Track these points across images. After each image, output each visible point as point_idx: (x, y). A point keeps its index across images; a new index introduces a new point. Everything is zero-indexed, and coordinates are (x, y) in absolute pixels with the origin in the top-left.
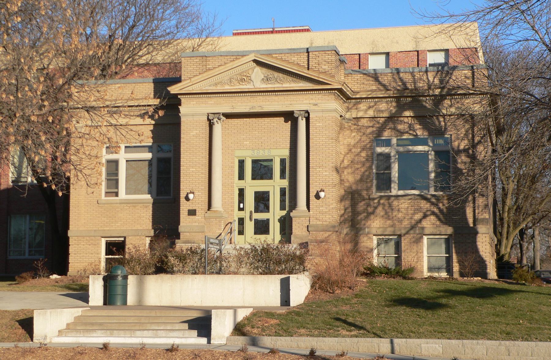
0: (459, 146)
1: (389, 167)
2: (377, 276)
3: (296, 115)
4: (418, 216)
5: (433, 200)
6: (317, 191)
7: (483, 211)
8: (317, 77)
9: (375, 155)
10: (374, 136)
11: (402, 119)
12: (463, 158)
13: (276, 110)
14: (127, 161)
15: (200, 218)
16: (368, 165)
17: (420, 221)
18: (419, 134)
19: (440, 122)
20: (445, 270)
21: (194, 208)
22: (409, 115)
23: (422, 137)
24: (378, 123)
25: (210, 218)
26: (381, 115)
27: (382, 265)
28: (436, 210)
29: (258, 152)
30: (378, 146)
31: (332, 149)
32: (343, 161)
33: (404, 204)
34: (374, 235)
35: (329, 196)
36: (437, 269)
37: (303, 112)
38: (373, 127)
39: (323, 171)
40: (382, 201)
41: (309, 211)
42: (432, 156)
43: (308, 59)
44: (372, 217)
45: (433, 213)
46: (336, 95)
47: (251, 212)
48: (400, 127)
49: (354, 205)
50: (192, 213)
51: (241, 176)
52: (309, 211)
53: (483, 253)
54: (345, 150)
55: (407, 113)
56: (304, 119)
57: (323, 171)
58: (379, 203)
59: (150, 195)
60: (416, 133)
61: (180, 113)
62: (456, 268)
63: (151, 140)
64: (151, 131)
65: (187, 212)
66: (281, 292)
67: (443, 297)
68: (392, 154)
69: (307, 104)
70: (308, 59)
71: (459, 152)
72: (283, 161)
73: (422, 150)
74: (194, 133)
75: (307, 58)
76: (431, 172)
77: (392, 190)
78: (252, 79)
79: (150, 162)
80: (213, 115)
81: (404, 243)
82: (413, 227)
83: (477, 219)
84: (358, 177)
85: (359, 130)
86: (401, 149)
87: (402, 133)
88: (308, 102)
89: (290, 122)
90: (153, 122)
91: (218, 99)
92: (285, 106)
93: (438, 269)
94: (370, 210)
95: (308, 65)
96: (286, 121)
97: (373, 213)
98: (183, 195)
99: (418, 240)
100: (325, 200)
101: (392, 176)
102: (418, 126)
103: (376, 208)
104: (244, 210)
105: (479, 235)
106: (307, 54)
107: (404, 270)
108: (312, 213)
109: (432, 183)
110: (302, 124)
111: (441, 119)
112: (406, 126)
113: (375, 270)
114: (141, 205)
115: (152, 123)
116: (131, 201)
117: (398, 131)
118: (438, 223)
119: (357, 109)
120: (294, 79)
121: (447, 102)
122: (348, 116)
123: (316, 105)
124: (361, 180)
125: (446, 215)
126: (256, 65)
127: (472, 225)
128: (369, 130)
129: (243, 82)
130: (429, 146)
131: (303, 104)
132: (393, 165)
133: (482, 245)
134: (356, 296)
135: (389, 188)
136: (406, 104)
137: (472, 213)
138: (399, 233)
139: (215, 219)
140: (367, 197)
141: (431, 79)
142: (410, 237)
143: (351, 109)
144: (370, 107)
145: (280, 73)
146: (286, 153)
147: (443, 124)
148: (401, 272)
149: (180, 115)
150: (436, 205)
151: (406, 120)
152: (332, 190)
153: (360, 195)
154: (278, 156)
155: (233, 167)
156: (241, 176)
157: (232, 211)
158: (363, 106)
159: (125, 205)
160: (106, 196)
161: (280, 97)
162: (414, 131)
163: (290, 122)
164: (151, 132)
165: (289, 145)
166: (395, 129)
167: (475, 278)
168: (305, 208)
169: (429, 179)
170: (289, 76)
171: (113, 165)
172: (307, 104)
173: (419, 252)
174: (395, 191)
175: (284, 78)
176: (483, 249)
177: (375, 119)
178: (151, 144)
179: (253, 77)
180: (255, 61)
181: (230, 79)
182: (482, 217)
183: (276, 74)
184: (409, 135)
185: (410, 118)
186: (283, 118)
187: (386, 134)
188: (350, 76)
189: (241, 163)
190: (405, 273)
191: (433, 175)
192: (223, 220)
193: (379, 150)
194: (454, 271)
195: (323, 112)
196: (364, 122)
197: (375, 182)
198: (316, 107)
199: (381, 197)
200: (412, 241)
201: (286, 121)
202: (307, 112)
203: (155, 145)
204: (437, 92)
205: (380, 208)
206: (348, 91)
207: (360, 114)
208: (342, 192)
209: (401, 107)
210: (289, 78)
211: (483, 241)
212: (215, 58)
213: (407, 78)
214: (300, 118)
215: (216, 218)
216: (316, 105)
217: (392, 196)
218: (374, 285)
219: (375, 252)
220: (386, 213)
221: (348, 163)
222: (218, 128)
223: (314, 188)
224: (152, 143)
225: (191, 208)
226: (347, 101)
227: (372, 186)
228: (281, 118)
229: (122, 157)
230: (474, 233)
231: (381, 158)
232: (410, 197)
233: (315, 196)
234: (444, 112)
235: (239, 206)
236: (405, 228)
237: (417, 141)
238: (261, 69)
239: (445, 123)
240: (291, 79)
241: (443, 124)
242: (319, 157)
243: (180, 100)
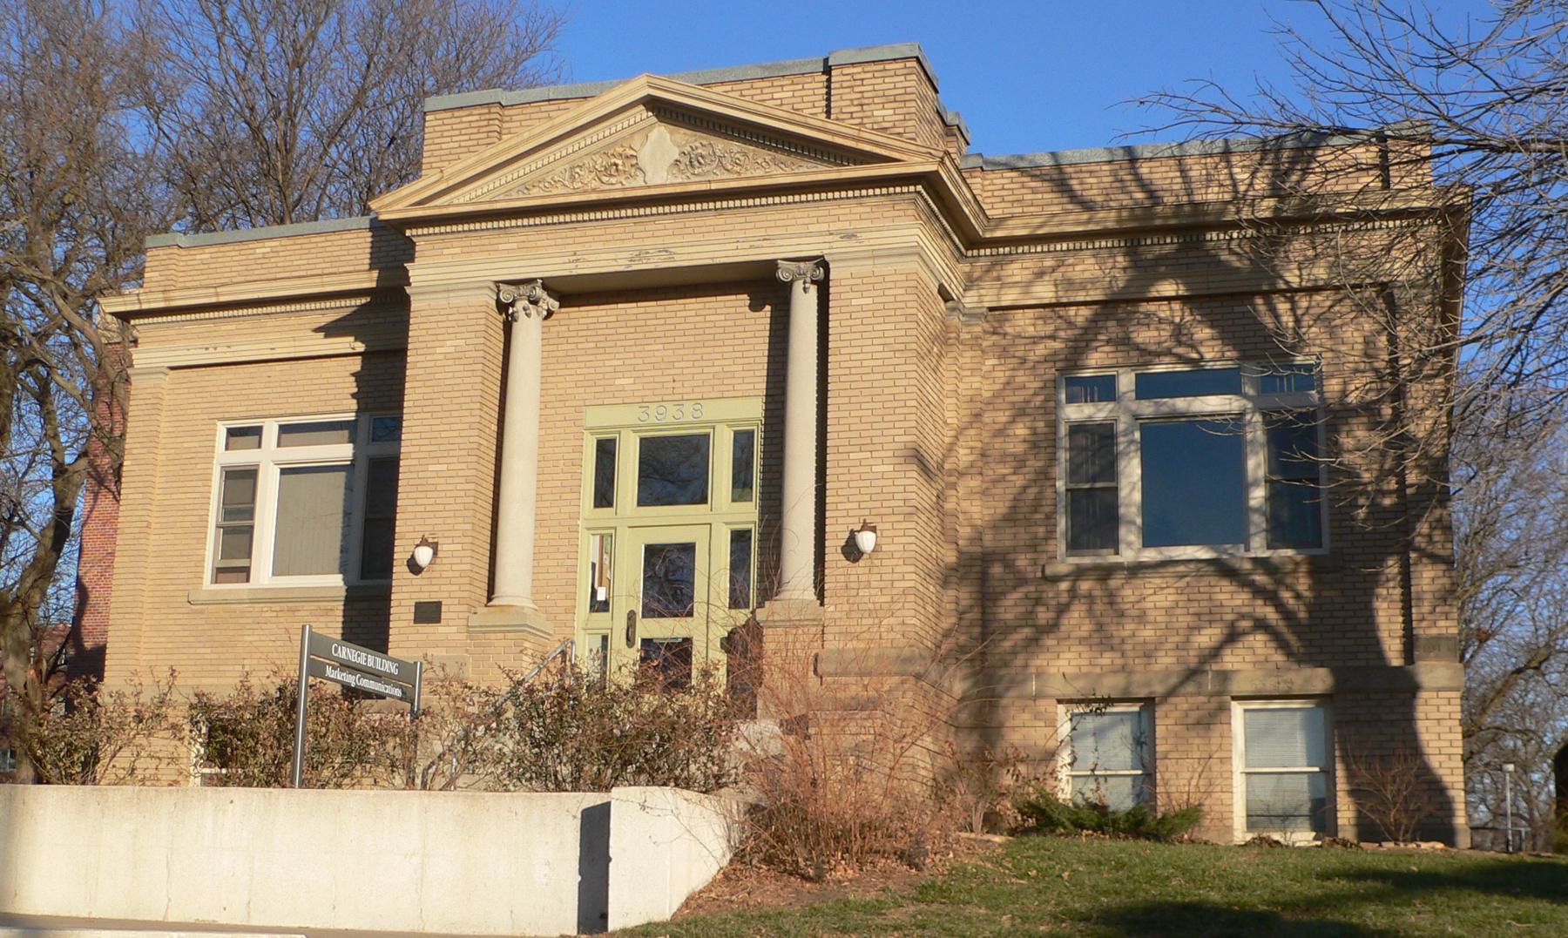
0: (1344, 393)
1: (1110, 470)
2: (1062, 834)
3: (783, 275)
4: (1207, 637)
5: (1260, 578)
6: (852, 532)
7: (1438, 610)
8: (853, 138)
9: (1063, 430)
10: (1059, 365)
11: (1152, 307)
12: (1361, 433)
13: (717, 261)
14: (284, 472)
15: (454, 629)
16: (1034, 464)
17: (1215, 653)
18: (1208, 356)
19: (1277, 317)
20: (1307, 824)
21: (434, 598)
22: (1173, 294)
23: (1219, 365)
24: (1071, 324)
25: (486, 630)
26: (1081, 297)
27: (1086, 800)
28: (1270, 613)
29: (662, 410)
30: (1071, 400)
31: (905, 382)
32: (951, 448)
33: (1157, 596)
34: (1060, 702)
35: (892, 548)
36: (1277, 821)
37: (810, 265)
38: (1053, 337)
39: (871, 462)
40: (1085, 586)
41: (822, 604)
42: (1256, 432)
43: (829, 94)
44: (1050, 642)
45: (1261, 625)
46: (921, 202)
47: (631, 616)
48: (1144, 336)
49: (986, 598)
50: (428, 613)
51: (604, 497)
52: (822, 604)
53: (1442, 758)
54: (962, 412)
55: (1168, 288)
56: (813, 290)
57: (871, 462)
58: (1073, 594)
59: (341, 576)
60: (1198, 352)
61: (409, 284)
62: (1346, 813)
63: (353, 404)
64: (353, 375)
65: (413, 609)
66: (580, 873)
67: (1366, 898)
68: (1121, 427)
69: (821, 233)
70: (829, 94)
71: (1341, 414)
72: (743, 441)
73: (1218, 408)
74: (449, 346)
75: (824, 103)
76: (1256, 484)
77: (1122, 547)
78: (640, 165)
79: (349, 469)
80: (512, 288)
81: (1165, 725)
82: (1192, 674)
83: (1417, 637)
84: (1002, 508)
85: (1004, 353)
86: (1147, 408)
87: (1150, 354)
88: (824, 227)
89: (768, 308)
90: (360, 347)
91: (533, 236)
92: (746, 245)
93: (1285, 818)
94: (1044, 616)
95: (828, 107)
96: (755, 306)
97: (1053, 627)
98: (400, 555)
99: (1213, 718)
100: (877, 562)
101: (1121, 501)
102: (1203, 333)
103: (1062, 610)
104: (607, 611)
105: (1423, 695)
106: (825, 78)
107: (1163, 818)
108: (832, 608)
109: (1258, 521)
110: (805, 304)
111: (1283, 307)
112: (1166, 332)
113: (1055, 816)
114: (312, 606)
115: (358, 350)
116: (269, 595)
117: (1137, 347)
118: (1279, 658)
119: (999, 278)
120: (779, 156)
121: (1299, 247)
122: (970, 300)
123: (850, 236)
124: (1011, 518)
125: (1309, 626)
126: (655, 120)
127: (1396, 660)
128: (1041, 350)
129: (611, 175)
130: (1245, 396)
131: (810, 234)
132: (1122, 464)
133: (1438, 729)
134: (924, 893)
135: (1114, 544)
136: (1160, 260)
137: (1401, 619)
138: (1143, 693)
139: (500, 636)
140: (1033, 573)
141: (1242, 176)
142: (1186, 706)
143: (979, 279)
144: (1040, 274)
145: (732, 138)
146: (753, 410)
147: (1288, 320)
148: (1153, 824)
149: (408, 290)
150: (1271, 597)
151: (1163, 311)
152: (904, 525)
153: (1009, 565)
154: (729, 422)
155: (577, 463)
156: (604, 497)
157: (571, 610)
158: (1017, 271)
159: (266, 607)
160: (216, 581)
161: (730, 218)
162: (1193, 347)
163: (768, 308)
164: (353, 379)
165: (764, 386)
166: (1124, 342)
167: (1424, 845)
168: (810, 595)
169: (1249, 509)
170: (763, 146)
171: (242, 480)
172: (821, 233)
173: (1220, 759)
174: (1131, 550)
175: (745, 155)
176: (1442, 744)
177: (1061, 311)
178: (351, 416)
179: (644, 158)
180: (653, 104)
181: (572, 168)
182: (1434, 631)
183: (721, 145)
184: (1174, 359)
185: (1176, 306)
186: (745, 296)
187: (1097, 361)
188: (978, 174)
189: (606, 452)
190: (1168, 827)
191: (1258, 496)
192: (532, 638)
193: (1075, 412)
194: (1340, 822)
195: (874, 257)
196: (1023, 323)
197: (1062, 523)
198: (852, 243)
199: (1079, 573)
200: (1190, 721)
201: (755, 306)
202: (822, 263)
203: (365, 419)
204: (1265, 209)
205: (1077, 614)
206: (967, 202)
207: (1008, 298)
208: (951, 557)
209: (1145, 270)
210: (764, 155)
211: (1439, 716)
212: (529, 110)
213: (1162, 176)
214: (798, 286)
215: (505, 630)
216: (850, 236)
217: (1119, 567)
218: (1031, 853)
219: (1065, 757)
220: (1100, 627)
221: (971, 458)
222: (528, 328)
223: (840, 521)
224: (357, 412)
225: (424, 598)
226: (969, 253)
227: (1050, 535)
228: (739, 297)
229: (269, 458)
230: (1404, 688)
231: (1082, 441)
232: (1181, 568)
233: (843, 548)
234: (1293, 278)
235: (594, 593)
236: (1167, 673)
237: (1201, 381)
238: (671, 133)
239: (1295, 315)
240: (768, 158)
241: (1288, 320)
242: (861, 413)
243: (411, 244)
